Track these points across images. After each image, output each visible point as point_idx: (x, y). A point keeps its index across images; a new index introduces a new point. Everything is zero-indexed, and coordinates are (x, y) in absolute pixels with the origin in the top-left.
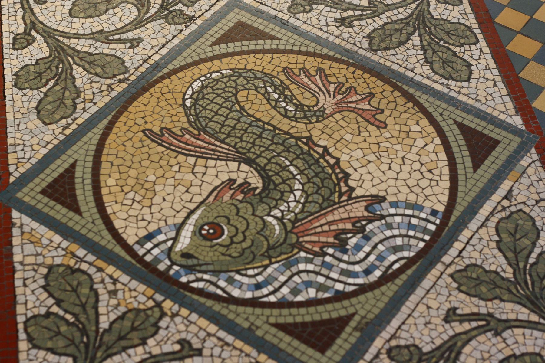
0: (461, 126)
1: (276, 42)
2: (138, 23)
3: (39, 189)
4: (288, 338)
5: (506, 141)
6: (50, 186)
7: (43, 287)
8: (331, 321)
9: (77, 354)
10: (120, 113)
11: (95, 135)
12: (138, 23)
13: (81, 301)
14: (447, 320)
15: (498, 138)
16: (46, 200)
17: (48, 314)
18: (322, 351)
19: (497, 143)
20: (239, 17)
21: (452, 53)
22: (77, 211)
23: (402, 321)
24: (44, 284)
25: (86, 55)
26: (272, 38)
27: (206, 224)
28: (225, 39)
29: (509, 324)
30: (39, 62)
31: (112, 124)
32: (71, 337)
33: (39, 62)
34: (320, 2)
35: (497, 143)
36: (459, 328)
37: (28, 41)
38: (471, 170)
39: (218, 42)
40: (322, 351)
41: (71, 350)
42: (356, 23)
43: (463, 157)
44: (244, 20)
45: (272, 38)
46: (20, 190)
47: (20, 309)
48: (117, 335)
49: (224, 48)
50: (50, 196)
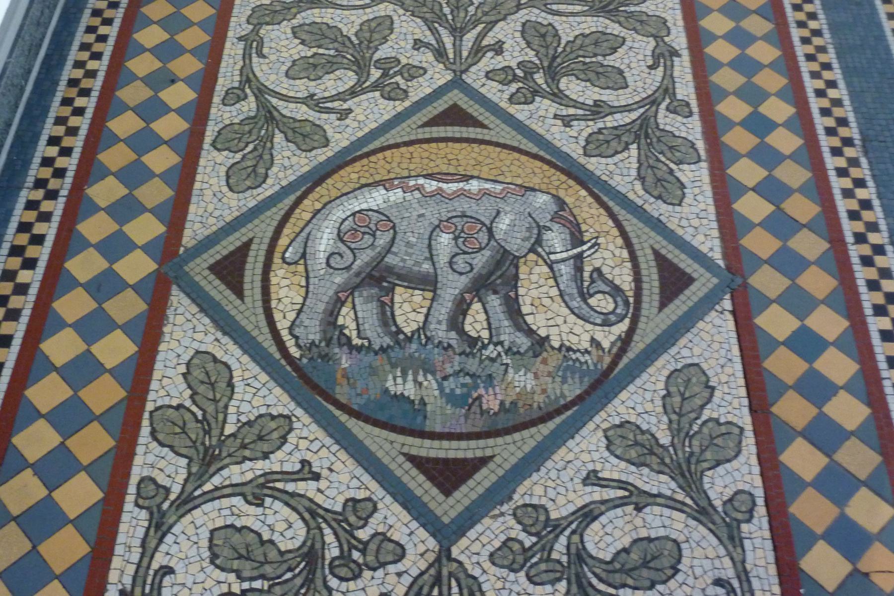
0: (657, 254)
2: (353, 93)
3: (206, 265)
4: (435, 129)
5: (703, 280)
6: (218, 263)
7: (184, 375)
9: (195, 457)
11: (276, 214)
12: (353, 93)
13: (215, 396)
14: (586, 481)
16: (212, 277)
17: (179, 407)
18: (447, 493)
20: (455, 99)
21: (293, 566)
24: (185, 371)
25: (291, 121)
26: (483, 126)
27: (370, 342)
28: (433, 122)
29: (654, 498)
32: (266, 438)
34: (575, 2)
36: (597, 494)
37: (238, 96)
39: (426, 125)
40: (447, 493)
41: (191, 452)
42: (575, 123)
43: (387, 453)
45: (483, 126)
47: (151, 396)
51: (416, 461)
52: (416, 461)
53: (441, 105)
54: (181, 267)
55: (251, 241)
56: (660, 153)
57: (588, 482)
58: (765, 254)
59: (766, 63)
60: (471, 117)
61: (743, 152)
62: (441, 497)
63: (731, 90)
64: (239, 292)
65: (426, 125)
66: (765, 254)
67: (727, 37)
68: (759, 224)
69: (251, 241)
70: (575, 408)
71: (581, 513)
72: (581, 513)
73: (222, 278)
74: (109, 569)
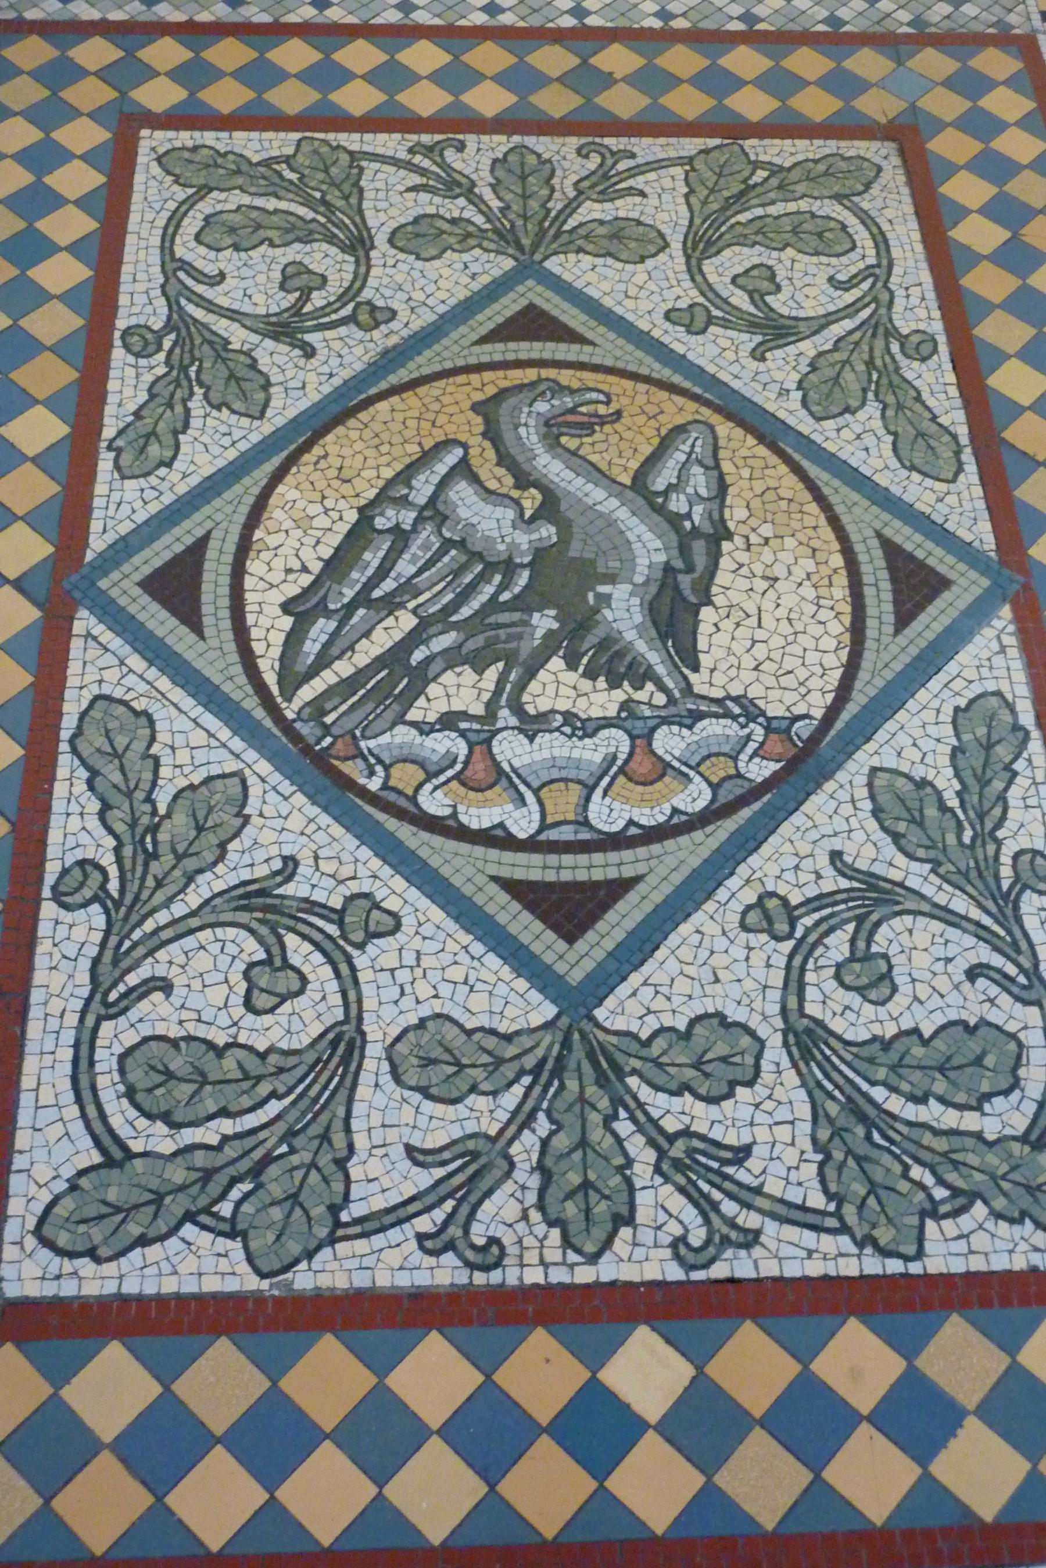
1: (587, 349)
8: (594, 886)
10: (306, 447)
15: (952, 575)
18: (571, 939)
19: (945, 583)
22: (197, 628)
23: (127, 768)
26: (581, 340)
30: (155, 391)
31: (292, 460)
33: (155, 391)
35: (945, 583)
38: (891, 629)
39: (483, 340)
40: (571, 939)
44: (539, 302)
46: (106, 574)
48: (649, 1101)
49: (496, 351)
50: (154, 595)
51: (514, 888)
52: (514, 888)
53: (509, 306)
54: (93, 584)
55: (206, 538)
56: (951, 810)
57: (741, 281)
58: (997, 298)
59: (1025, 162)
60: (530, 906)
61: (961, 162)
62: (561, 945)
63: (961, 163)
64: (195, 625)
65: (483, 340)
66: (997, 298)
67: (987, 211)
68: (1010, 357)
69: (206, 538)
70: (769, 796)
71: (802, 1065)
72: (802, 1065)
73: (166, 603)
74: (15, 1129)
